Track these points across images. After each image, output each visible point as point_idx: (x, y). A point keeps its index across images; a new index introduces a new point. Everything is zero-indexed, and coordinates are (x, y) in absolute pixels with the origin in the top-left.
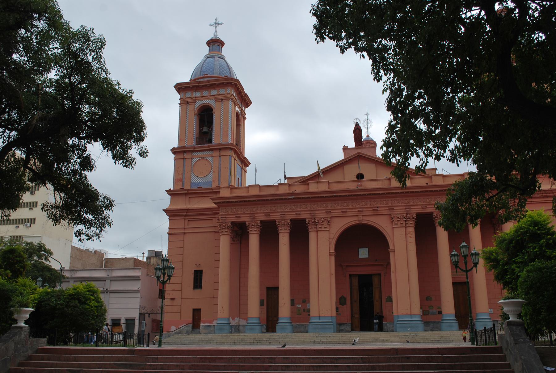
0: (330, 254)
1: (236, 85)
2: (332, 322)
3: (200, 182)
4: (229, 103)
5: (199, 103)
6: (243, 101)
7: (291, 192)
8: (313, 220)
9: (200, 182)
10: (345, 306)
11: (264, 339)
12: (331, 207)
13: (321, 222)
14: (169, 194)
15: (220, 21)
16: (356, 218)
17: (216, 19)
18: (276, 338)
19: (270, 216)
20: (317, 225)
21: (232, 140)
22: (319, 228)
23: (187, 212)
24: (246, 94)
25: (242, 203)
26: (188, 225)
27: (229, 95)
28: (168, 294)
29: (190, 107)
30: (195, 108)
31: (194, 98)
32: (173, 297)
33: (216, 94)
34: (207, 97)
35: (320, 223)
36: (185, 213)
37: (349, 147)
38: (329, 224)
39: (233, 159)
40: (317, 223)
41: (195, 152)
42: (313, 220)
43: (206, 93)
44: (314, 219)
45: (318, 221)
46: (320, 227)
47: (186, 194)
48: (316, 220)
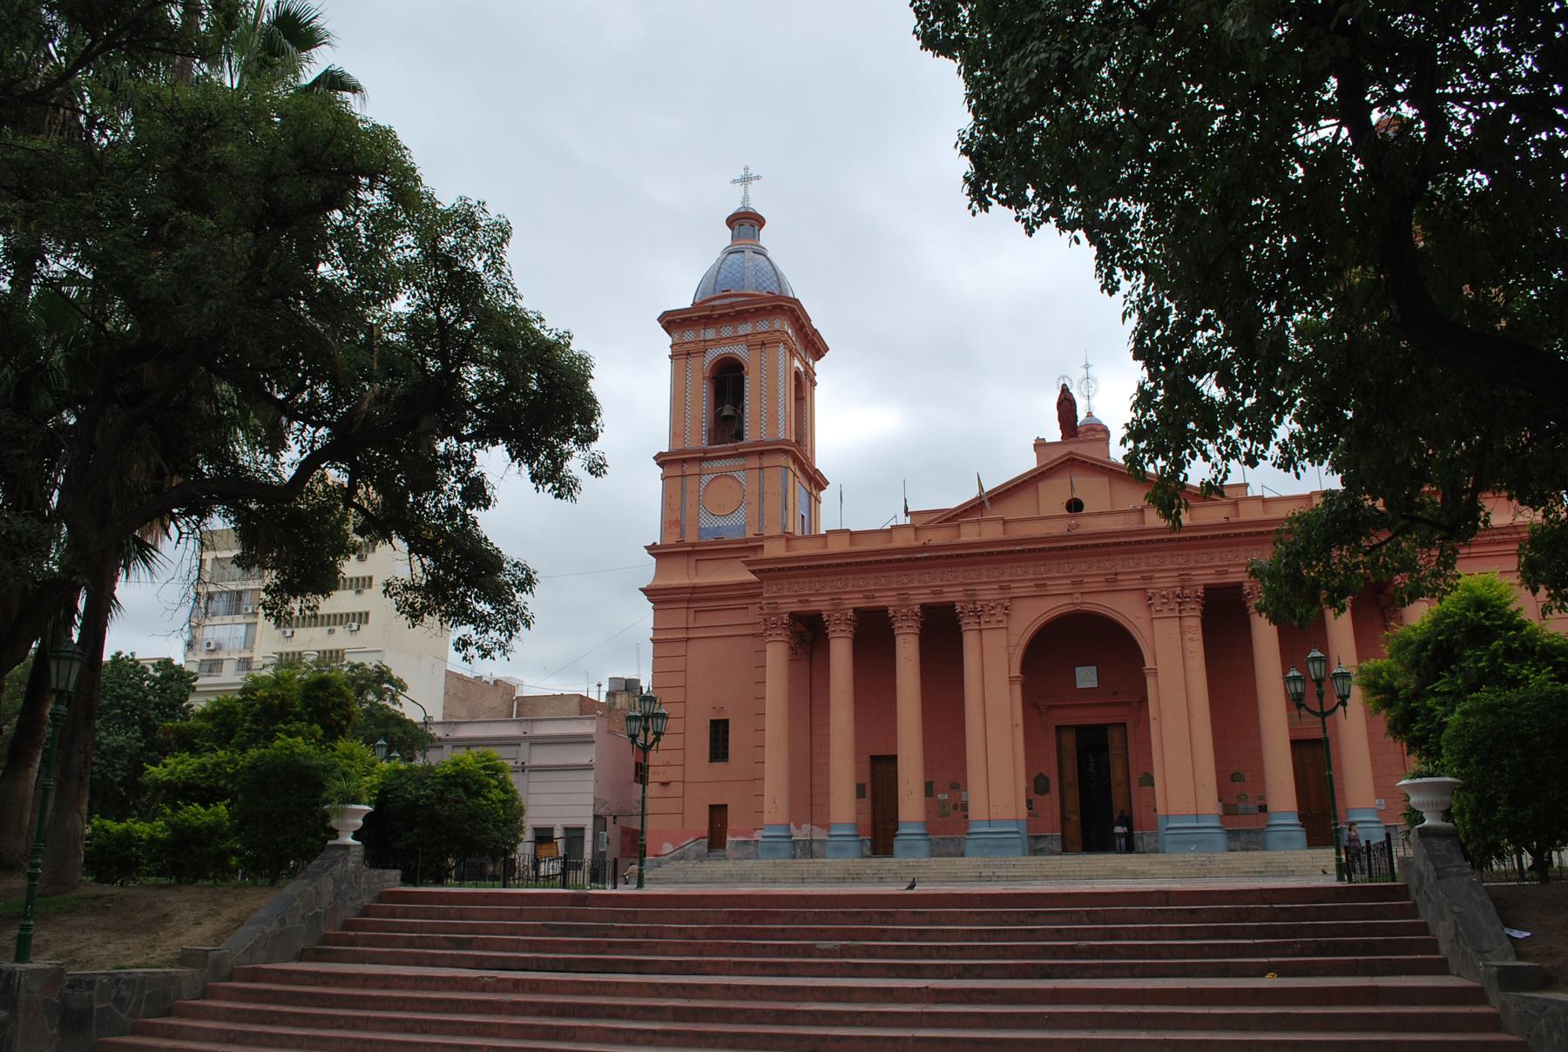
0: (1012, 680)
2: (1017, 832)
5: (714, 354)
7: (920, 543)
8: (971, 606)
10: (1047, 795)
11: (868, 871)
14: (653, 555)
15: (753, 172)
16: (1067, 600)
17: (746, 169)
19: (874, 597)
20: (979, 617)
21: (788, 432)
23: (691, 594)
27: (778, 334)
28: (654, 773)
29: (694, 363)
31: (702, 344)
38: (1007, 614)
39: (791, 474)
42: (971, 606)
43: (727, 331)
44: (974, 602)
47: (689, 553)
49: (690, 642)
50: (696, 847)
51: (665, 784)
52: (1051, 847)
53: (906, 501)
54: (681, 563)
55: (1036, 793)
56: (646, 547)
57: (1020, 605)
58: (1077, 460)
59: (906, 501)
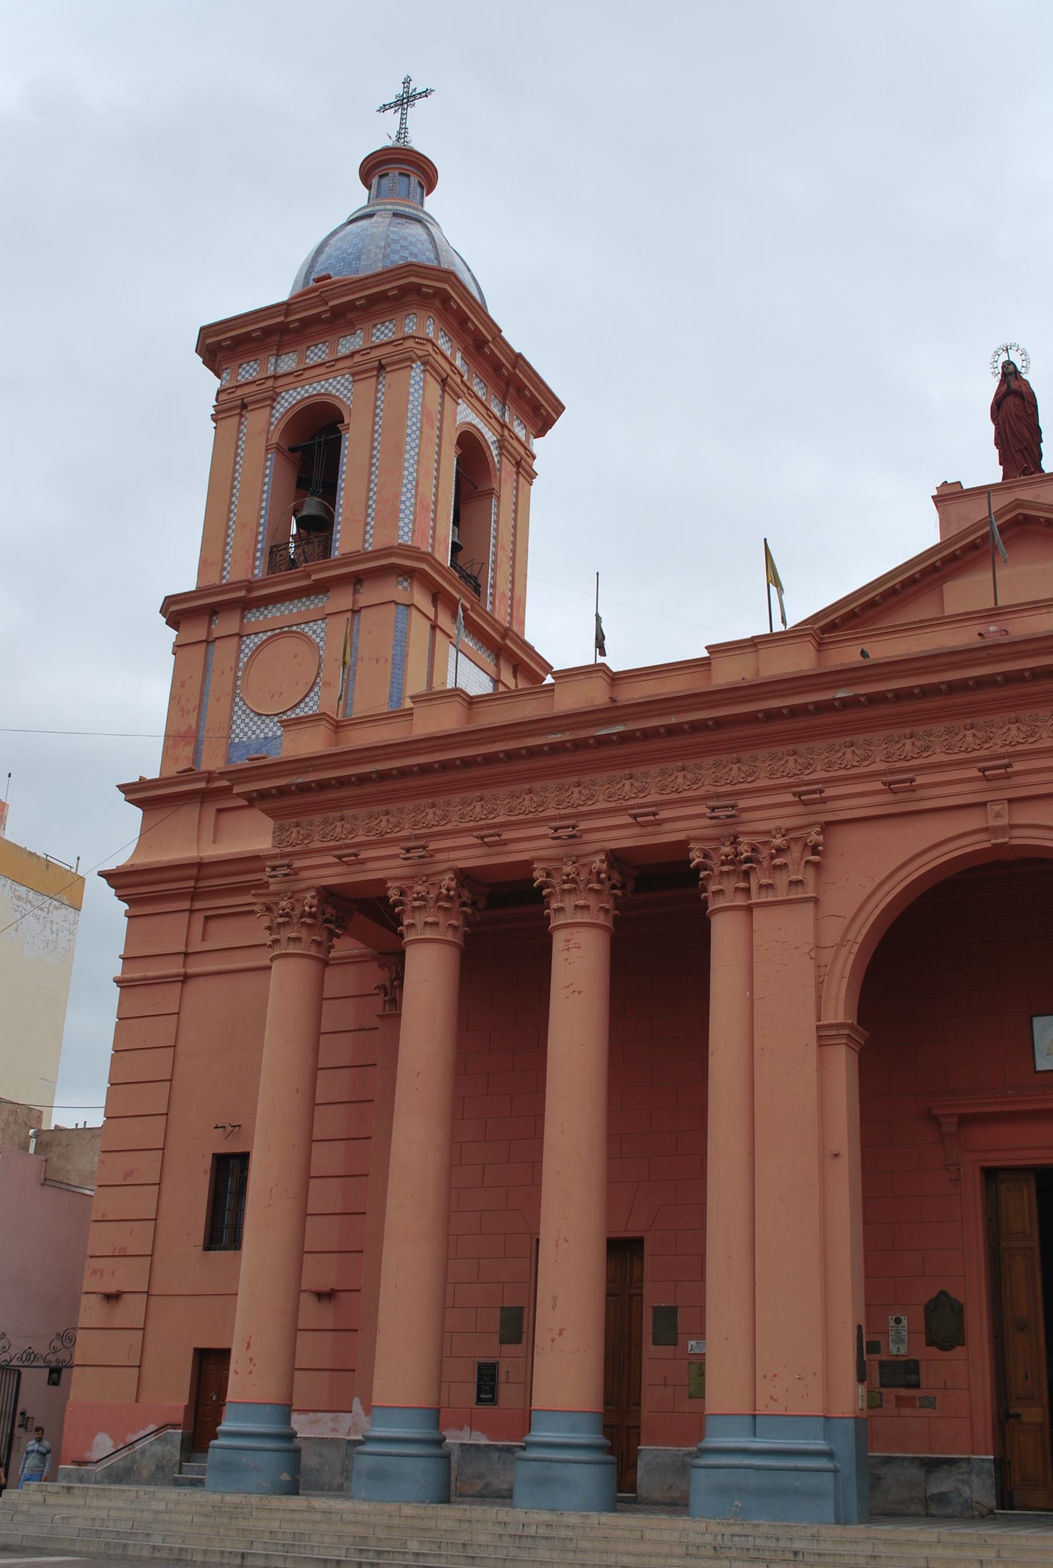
0: (824, 1035)
1: (445, 298)
2: (829, 1455)
3: (266, 738)
4: (410, 377)
5: (291, 398)
6: (511, 390)
8: (726, 849)
9: (266, 738)
10: (958, 1352)
12: (829, 766)
13: (772, 857)
14: (123, 792)
16: (972, 821)
17: (407, 82)
18: (483, 1539)
19: (505, 843)
20: (746, 875)
22: (761, 886)
23: (197, 879)
24: (520, 356)
25: (369, 789)
26: (203, 940)
27: (410, 343)
28: (95, 1272)
30: (271, 424)
31: (270, 383)
32: (112, 1289)
33: (357, 347)
34: (322, 370)
35: (765, 864)
36: (192, 883)
37: (965, 487)
38: (817, 865)
39: (419, 628)
40: (748, 860)
41: (258, 607)
42: (726, 849)
43: (318, 354)
44: (735, 842)
45: (754, 849)
46: (764, 881)
48: (742, 848)
49: (192, 986)
50: (158, 1448)
51: (112, 1297)
52: (966, 1491)
53: (598, 619)
54: (189, 814)
55: (930, 1343)
56: (120, 787)
57: (848, 840)
58: (1036, 519)
59: (598, 619)
